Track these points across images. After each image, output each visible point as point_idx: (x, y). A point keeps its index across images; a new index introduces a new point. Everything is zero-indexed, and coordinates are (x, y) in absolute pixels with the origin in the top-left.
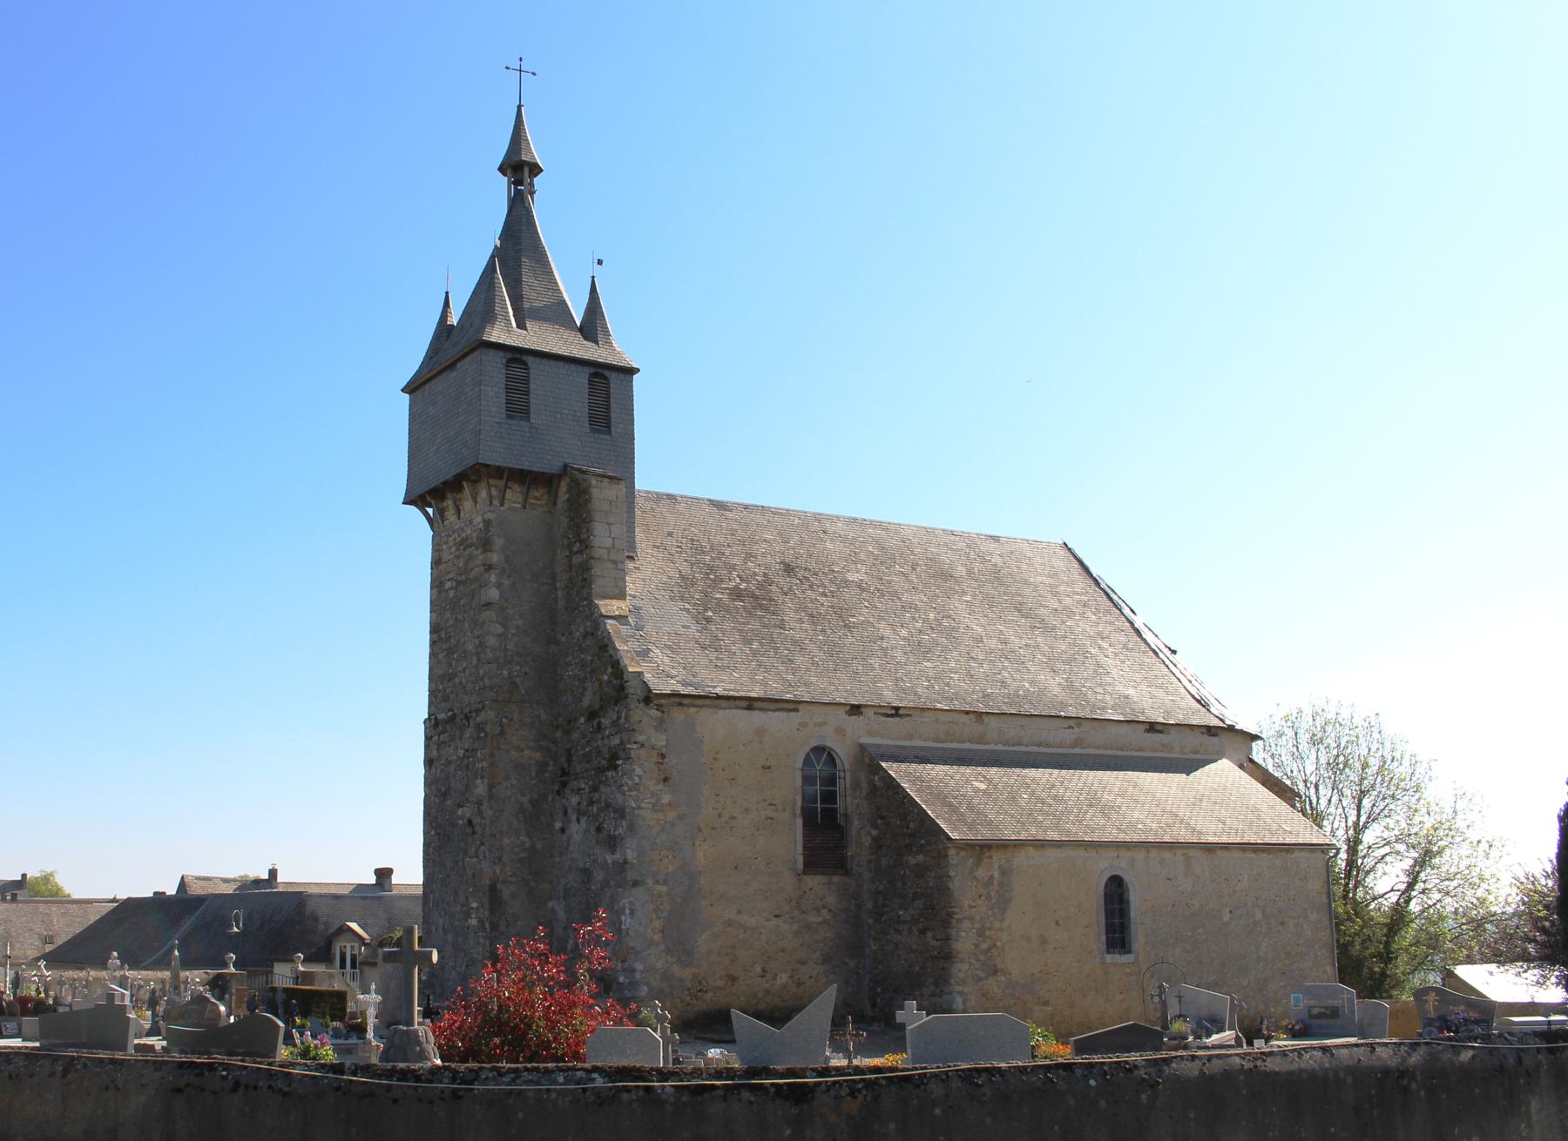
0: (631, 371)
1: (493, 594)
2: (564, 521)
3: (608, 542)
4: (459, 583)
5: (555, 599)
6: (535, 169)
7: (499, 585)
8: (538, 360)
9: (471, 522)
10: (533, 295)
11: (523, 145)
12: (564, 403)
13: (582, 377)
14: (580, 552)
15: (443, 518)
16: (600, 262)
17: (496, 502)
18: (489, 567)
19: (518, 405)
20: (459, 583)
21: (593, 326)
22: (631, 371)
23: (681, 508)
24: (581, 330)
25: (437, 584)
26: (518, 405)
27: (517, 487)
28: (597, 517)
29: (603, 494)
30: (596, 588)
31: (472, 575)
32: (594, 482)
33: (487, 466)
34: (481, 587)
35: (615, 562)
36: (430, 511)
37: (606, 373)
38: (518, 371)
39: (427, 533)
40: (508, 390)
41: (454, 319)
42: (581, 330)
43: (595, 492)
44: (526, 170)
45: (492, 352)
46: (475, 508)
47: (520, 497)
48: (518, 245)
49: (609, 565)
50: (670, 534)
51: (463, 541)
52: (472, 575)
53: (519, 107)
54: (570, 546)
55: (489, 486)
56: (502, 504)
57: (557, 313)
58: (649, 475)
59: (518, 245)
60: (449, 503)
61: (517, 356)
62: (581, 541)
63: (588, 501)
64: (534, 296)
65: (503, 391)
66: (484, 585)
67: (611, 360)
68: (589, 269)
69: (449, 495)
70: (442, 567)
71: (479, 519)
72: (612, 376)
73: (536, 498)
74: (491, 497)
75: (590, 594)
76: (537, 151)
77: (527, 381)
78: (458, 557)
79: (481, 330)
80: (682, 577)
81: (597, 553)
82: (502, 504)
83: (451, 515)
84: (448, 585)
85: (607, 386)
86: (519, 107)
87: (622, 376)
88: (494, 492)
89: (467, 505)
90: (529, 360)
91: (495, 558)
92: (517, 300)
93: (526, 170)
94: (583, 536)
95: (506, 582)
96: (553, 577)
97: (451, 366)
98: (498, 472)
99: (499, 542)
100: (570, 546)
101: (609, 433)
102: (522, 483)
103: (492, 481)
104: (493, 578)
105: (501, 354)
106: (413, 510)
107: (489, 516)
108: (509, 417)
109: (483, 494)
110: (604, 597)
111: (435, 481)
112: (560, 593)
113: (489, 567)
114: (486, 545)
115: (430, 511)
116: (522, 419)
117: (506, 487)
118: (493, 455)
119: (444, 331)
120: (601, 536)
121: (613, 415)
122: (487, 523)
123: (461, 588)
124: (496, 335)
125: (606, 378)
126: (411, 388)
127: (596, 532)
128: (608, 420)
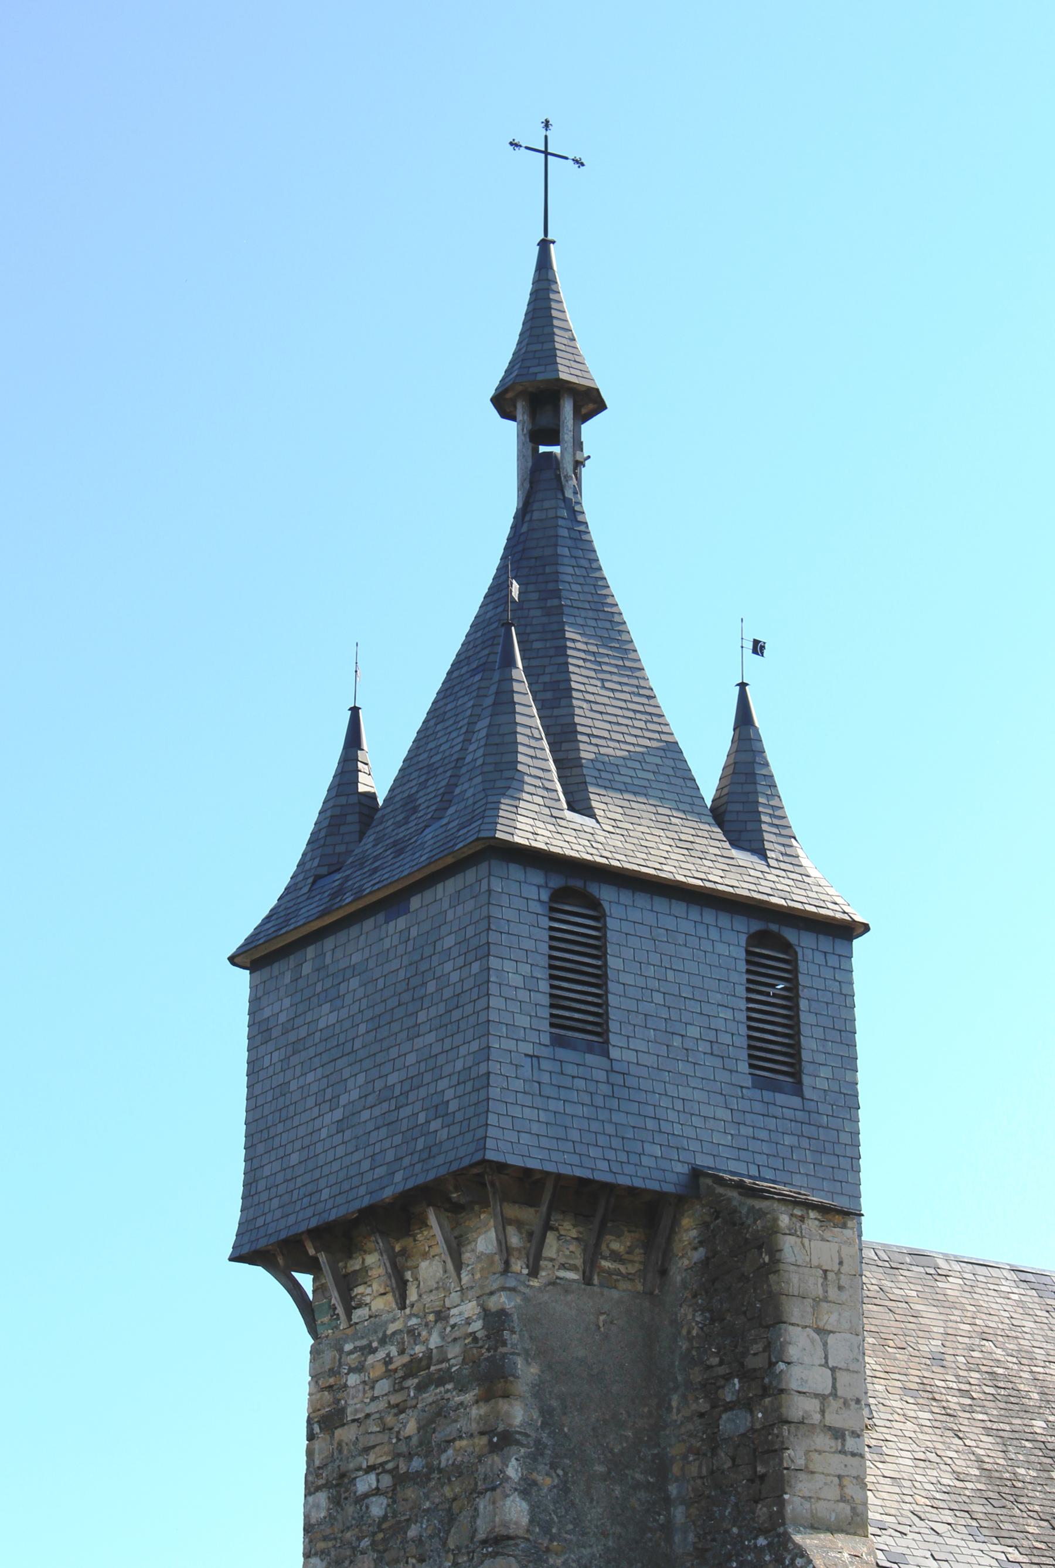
0: (848, 930)
1: (516, 1511)
2: (692, 1318)
3: (820, 1381)
4: (400, 1479)
5: (667, 1529)
6: (590, 402)
7: (527, 1488)
8: (626, 897)
9: (441, 1315)
10: (601, 727)
11: (560, 341)
12: (678, 998)
13: (729, 944)
14: (748, 1406)
15: (350, 1305)
16: (758, 648)
17: (519, 1266)
18: (502, 1440)
19: (580, 1014)
20: (400, 1479)
21: (744, 808)
22: (848, 930)
23: (951, 1286)
24: (719, 814)
25: (328, 1478)
26: (580, 1014)
27: (569, 1229)
28: (795, 1311)
29: (804, 1249)
30: (796, 1501)
31: (446, 1458)
32: (784, 1220)
33: (501, 1167)
34: (475, 1493)
35: (838, 1434)
36: (306, 1281)
37: (790, 935)
38: (580, 926)
39: (300, 1340)
40: (556, 970)
41: (377, 779)
42: (719, 814)
43: (789, 1246)
44: (567, 409)
45: (516, 871)
46: (450, 1286)
47: (575, 1254)
48: (546, 594)
49: (823, 1441)
50: (938, 1359)
51: (413, 1368)
52: (446, 1458)
53: (545, 245)
54: (710, 1388)
55: (505, 1222)
56: (534, 1273)
57: (660, 771)
58: (895, 1204)
59: (546, 594)
60: (373, 1261)
61: (577, 884)
62: (747, 1376)
63: (774, 1266)
64: (600, 732)
65: (542, 974)
66: (494, 1485)
67: (801, 900)
68: (729, 667)
69: (376, 1242)
70: (346, 1434)
71: (471, 1308)
72: (804, 942)
73: (615, 1257)
74: (503, 1244)
75: (778, 1518)
76: (595, 347)
77: (600, 950)
78: (400, 1409)
79: (488, 812)
80: (987, 1474)
81: (801, 1407)
82: (534, 1273)
83: (375, 1299)
84: (365, 1484)
85: (791, 961)
86: (545, 245)
87: (825, 943)
88: (515, 1240)
89: (430, 1270)
90: (606, 894)
91: (518, 1414)
92: (562, 735)
93: (567, 409)
94: (751, 1363)
95: (546, 1481)
96: (661, 1468)
97: (393, 903)
98: (527, 1185)
99: (527, 1372)
100: (710, 1388)
101: (797, 1089)
102: (581, 1217)
103: (512, 1211)
104: (513, 1471)
105: (537, 877)
106: (258, 1276)
107: (502, 1301)
108: (558, 1041)
109: (484, 1242)
110: (816, 1526)
111: (335, 1205)
112: (679, 1513)
113: (502, 1440)
114: (491, 1378)
115: (306, 1281)
116: (590, 1049)
117: (547, 1227)
118: (522, 1135)
119: (347, 809)
120: (804, 1366)
121: (808, 1044)
122: (496, 1322)
123: (411, 1492)
124: (535, 822)
125: (595, 904)
126: (256, 955)
127: (793, 1352)
128: (794, 1051)
